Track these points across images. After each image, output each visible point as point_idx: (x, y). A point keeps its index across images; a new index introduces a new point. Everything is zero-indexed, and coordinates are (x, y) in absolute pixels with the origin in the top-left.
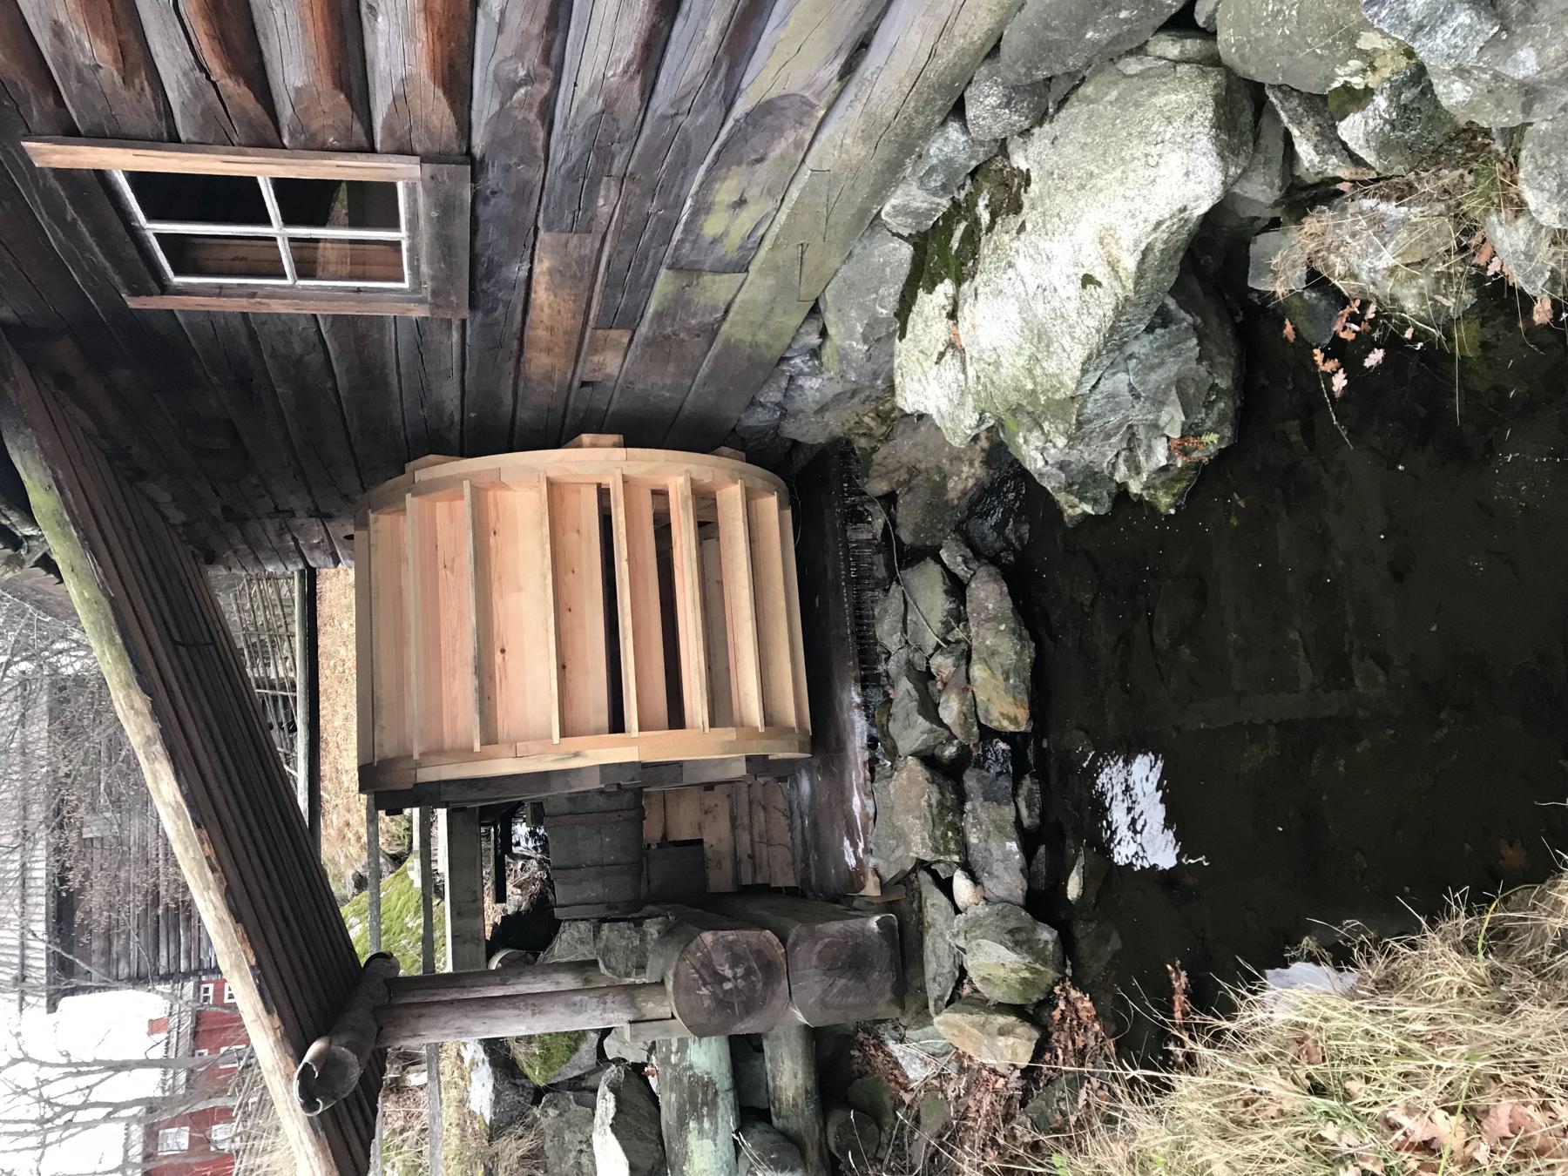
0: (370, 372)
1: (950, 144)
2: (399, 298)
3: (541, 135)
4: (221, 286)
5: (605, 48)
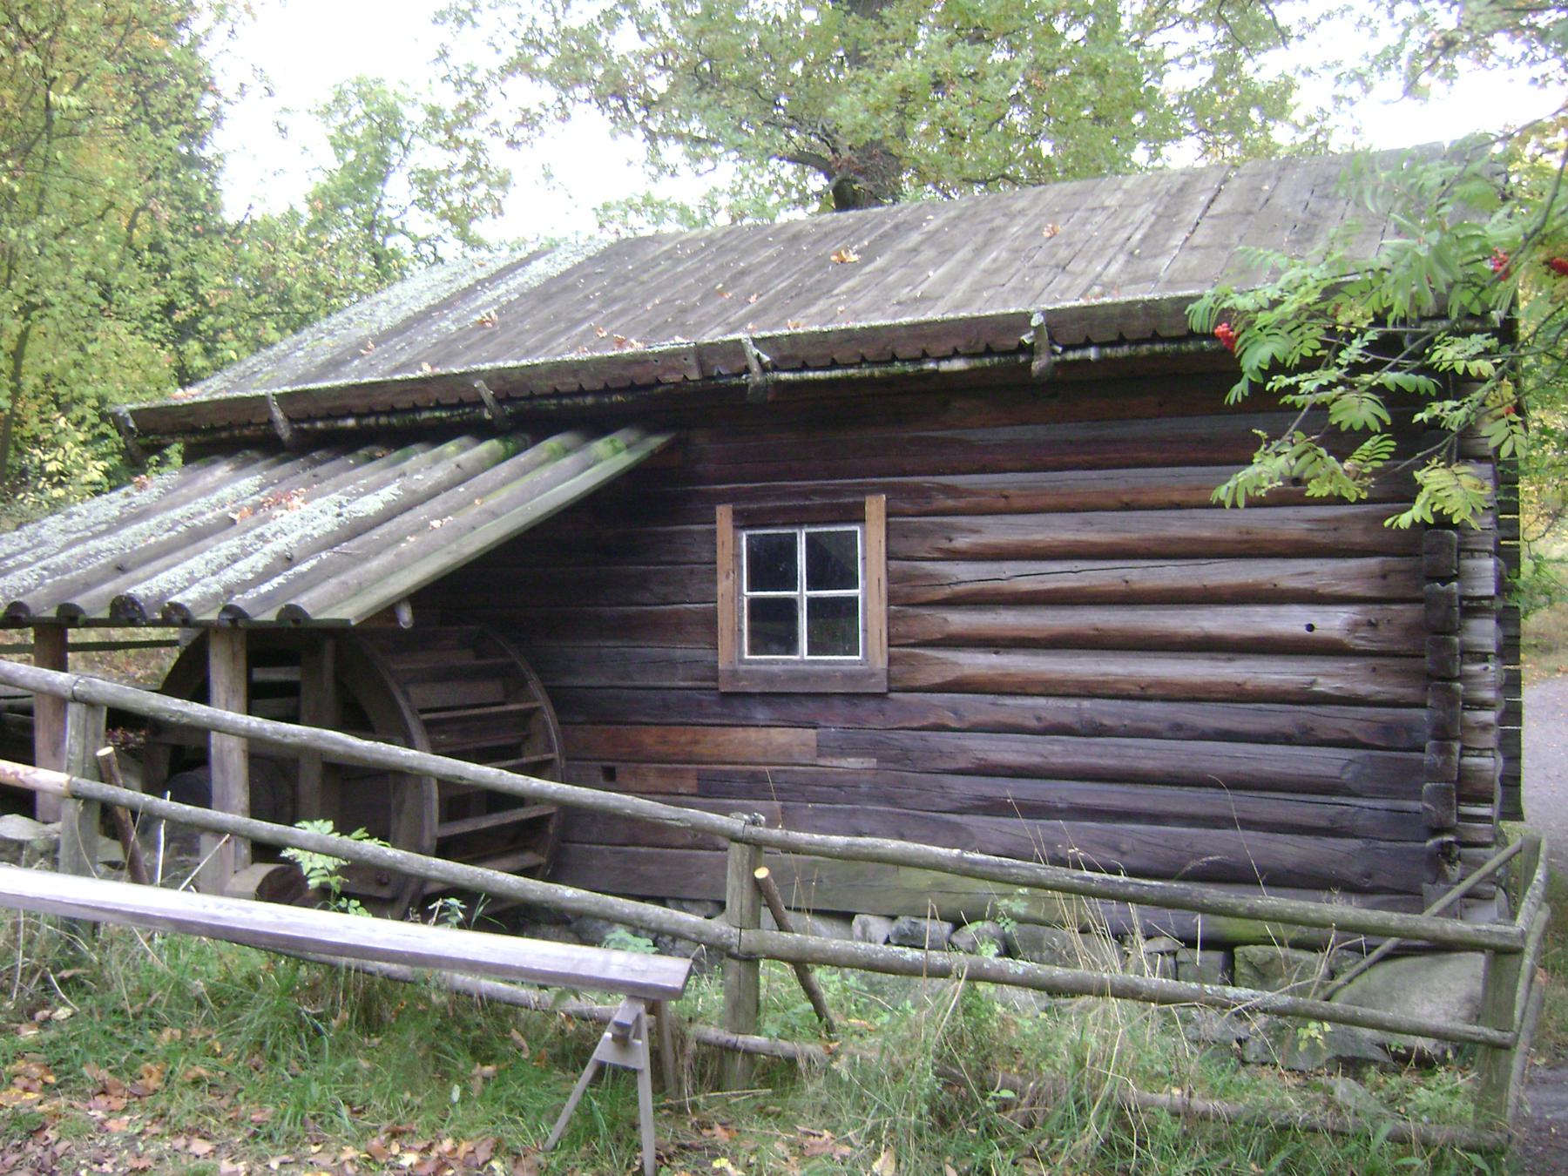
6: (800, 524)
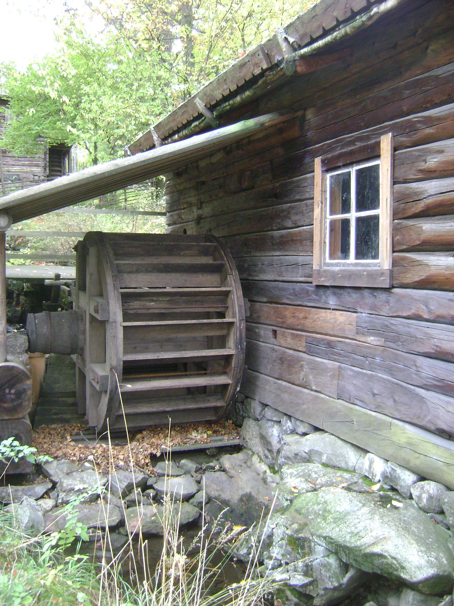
0: (284, 244)
1: (407, 478)
2: (323, 260)
3: (405, 314)
4: (325, 191)
5: (446, 338)
6: (351, 164)
